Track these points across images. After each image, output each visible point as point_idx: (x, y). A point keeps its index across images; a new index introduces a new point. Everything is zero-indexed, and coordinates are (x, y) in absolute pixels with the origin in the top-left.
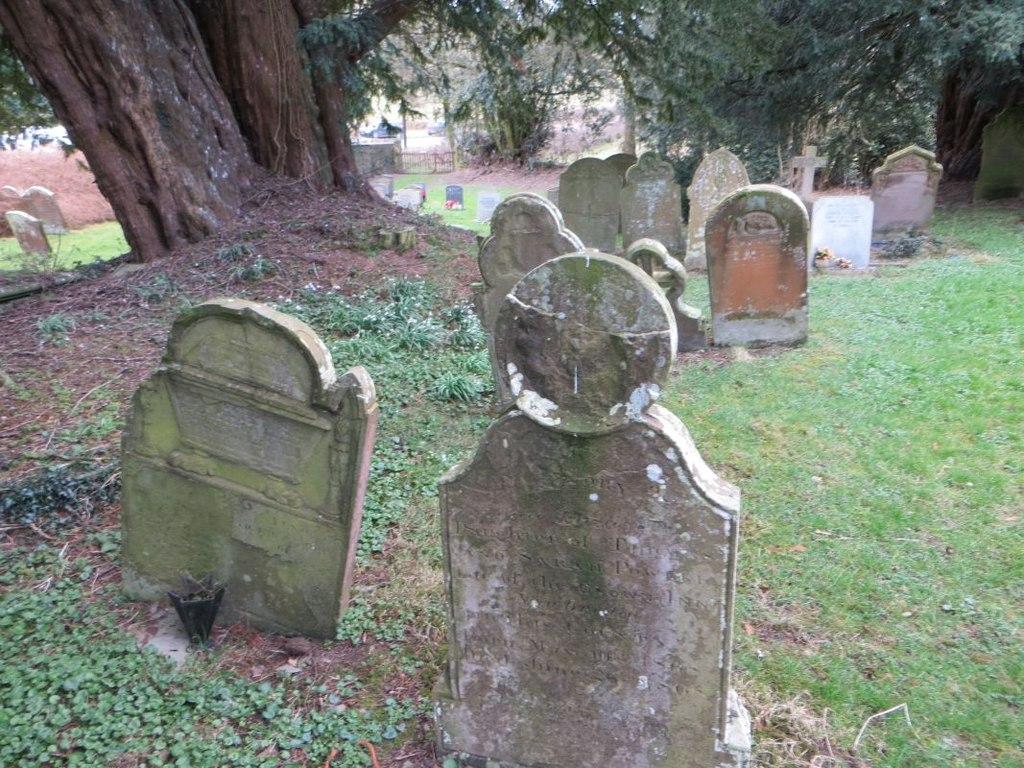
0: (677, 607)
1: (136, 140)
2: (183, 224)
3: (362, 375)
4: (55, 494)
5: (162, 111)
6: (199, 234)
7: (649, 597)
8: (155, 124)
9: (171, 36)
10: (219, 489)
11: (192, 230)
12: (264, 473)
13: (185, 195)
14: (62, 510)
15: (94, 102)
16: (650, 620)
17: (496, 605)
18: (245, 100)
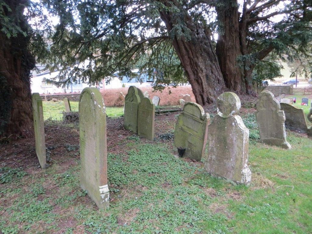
0: (236, 146)
1: (201, 82)
2: (208, 100)
3: (208, 115)
4: (168, 136)
5: (207, 76)
6: (211, 102)
7: (233, 144)
8: (205, 79)
9: (211, 61)
10: (187, 132)
11: (210, 101)
12: (193, 130)
13: (209, 94)
14: (169, 139)
15: (194, 75)
16: (232, 149)
17: (214, 145)
18: (226, 74)
